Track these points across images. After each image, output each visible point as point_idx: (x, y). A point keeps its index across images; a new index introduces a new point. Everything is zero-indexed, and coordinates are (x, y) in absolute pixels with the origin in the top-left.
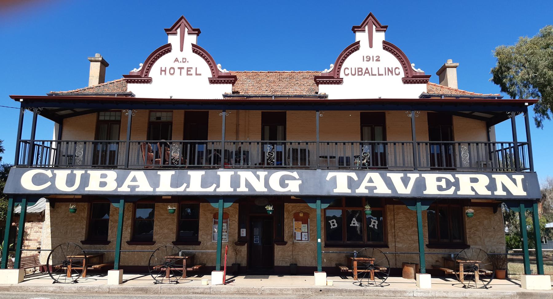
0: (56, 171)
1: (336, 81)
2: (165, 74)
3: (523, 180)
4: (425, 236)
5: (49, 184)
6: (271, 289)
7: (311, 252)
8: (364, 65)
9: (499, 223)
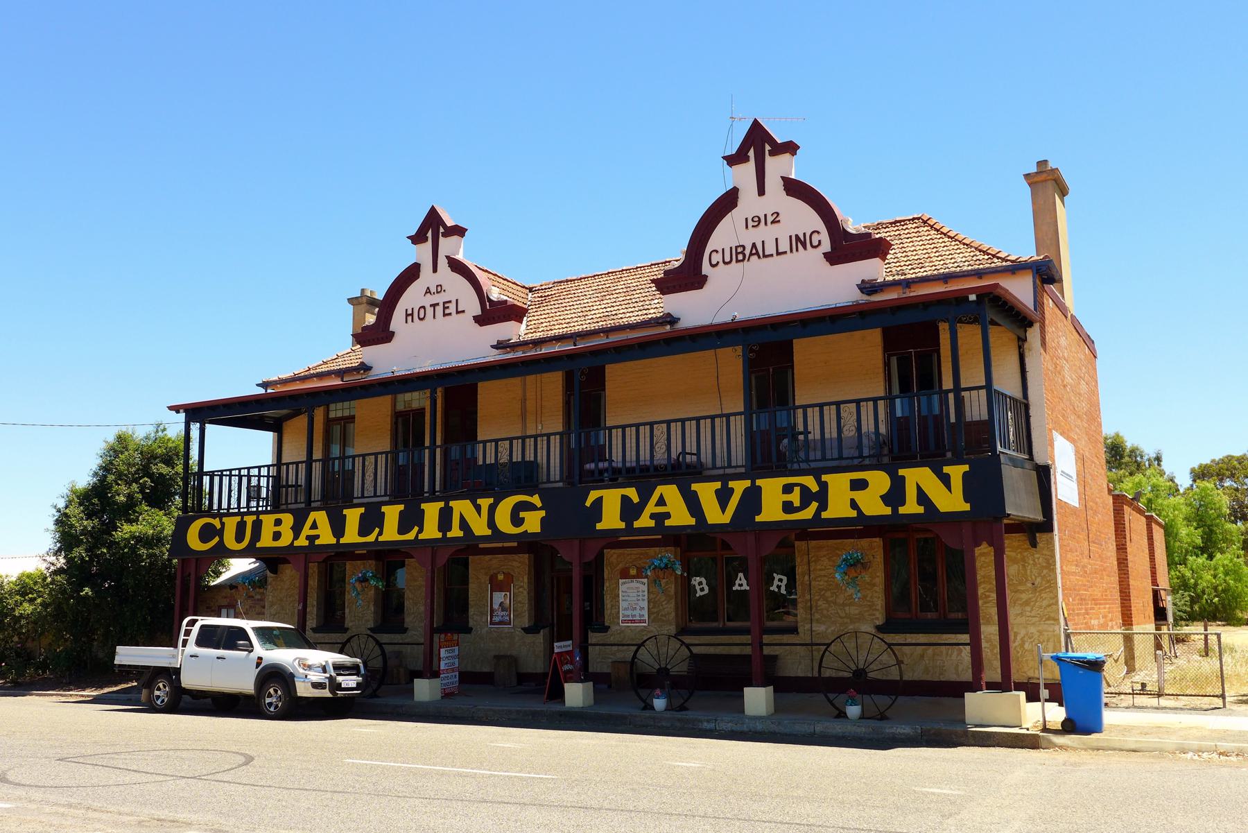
2: (412, 321)
4: (874, 607)
5: (217, 539)
8: (749, 238)
9: (1045, 571)
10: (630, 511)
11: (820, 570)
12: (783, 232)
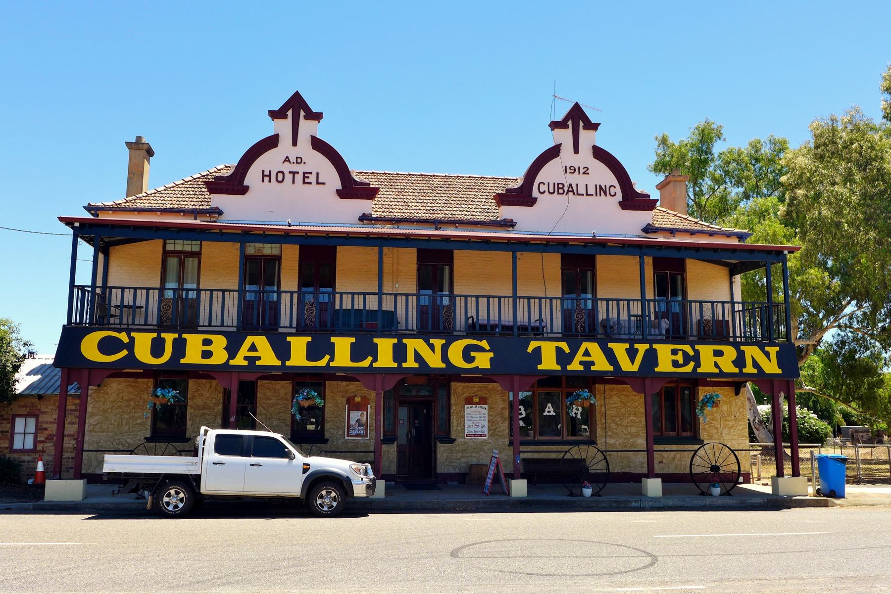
2: (270, 181)
5: (125, 353)
7: (489, 453)
9: (741, 410)
10: (563, 358)
11: (612, 404)
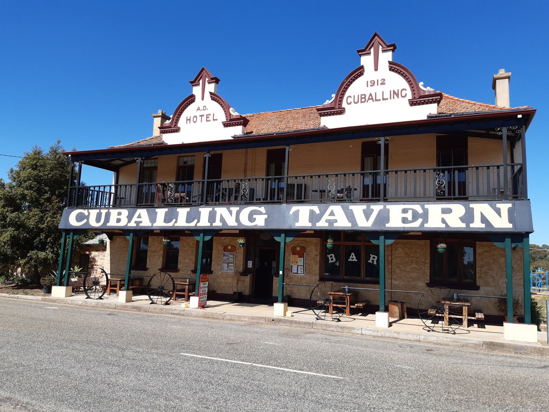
0: (90, 211)
1: (337, 111)
3: (510, 211)
4: (426, 274)
5: (85, 221)
6: (230, 315)
8: (368, 91)
10: (313, 217)
11: (398, 254)
12: (387, 89)
